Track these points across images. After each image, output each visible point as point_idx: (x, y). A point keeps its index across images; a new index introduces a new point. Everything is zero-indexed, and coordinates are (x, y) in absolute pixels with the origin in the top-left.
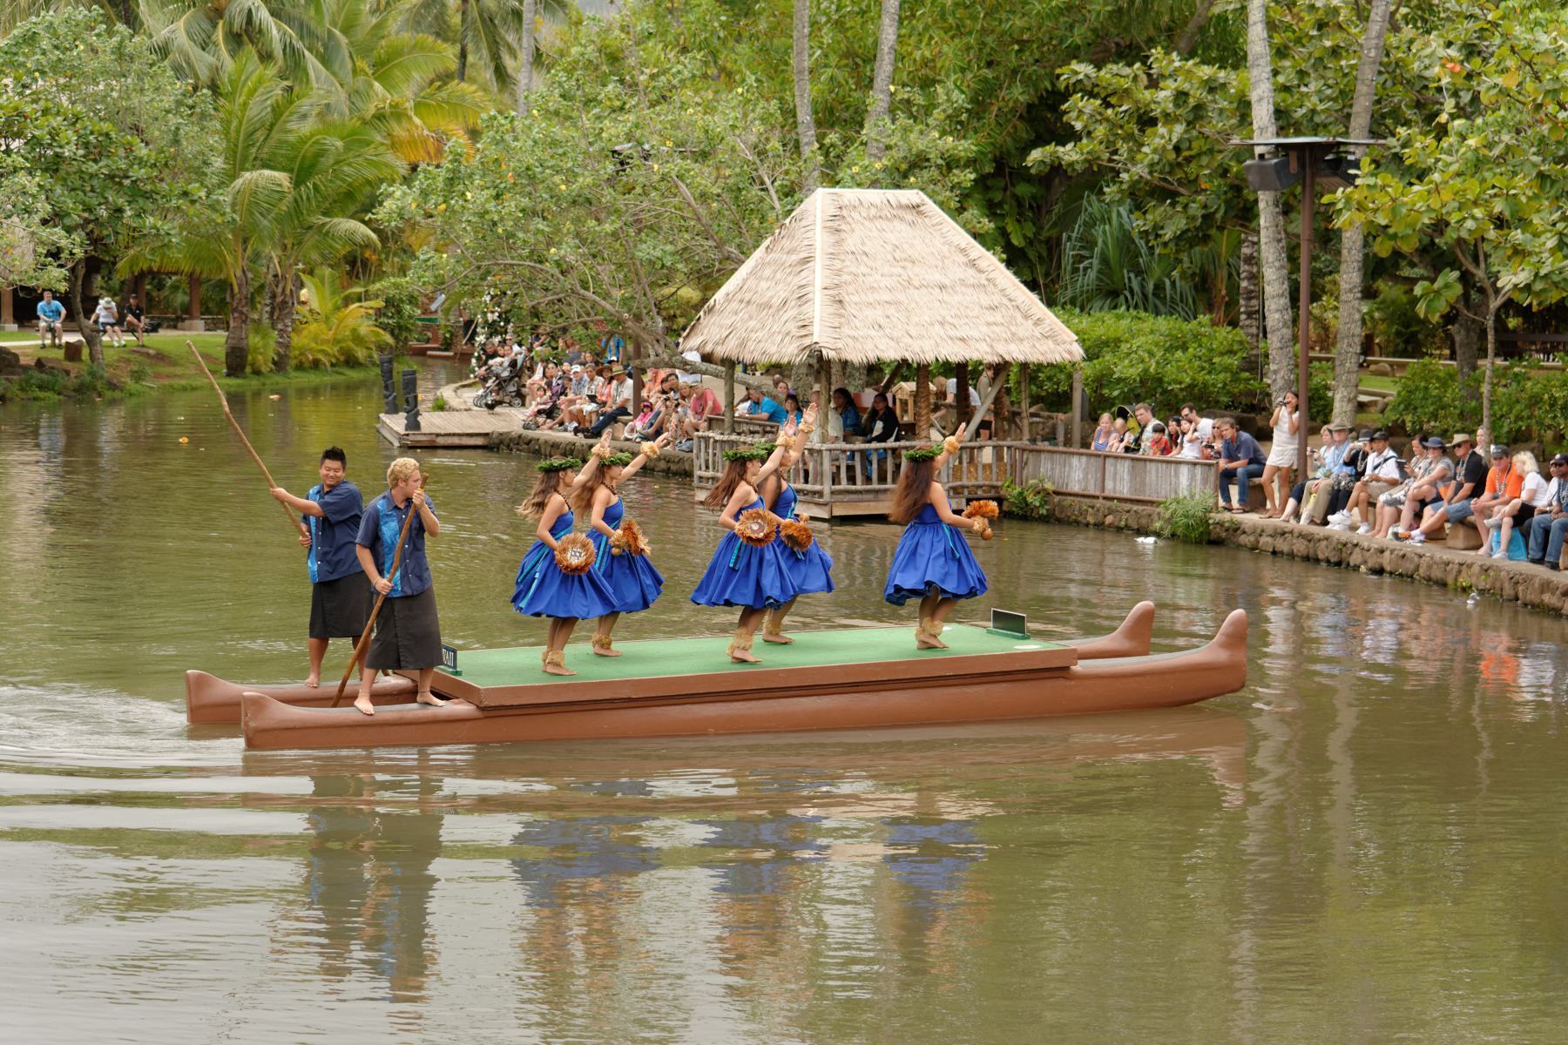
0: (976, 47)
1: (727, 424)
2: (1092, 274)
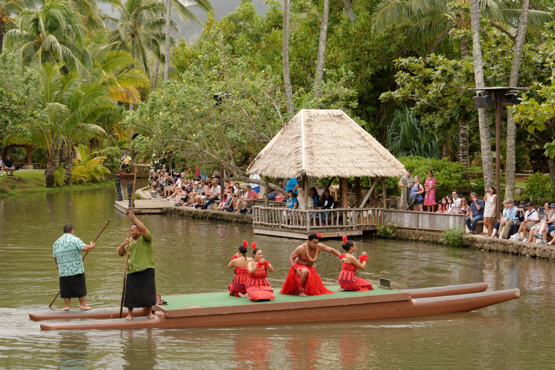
0: (352, 53)
1: (266, 203)
2: (399, 142)
